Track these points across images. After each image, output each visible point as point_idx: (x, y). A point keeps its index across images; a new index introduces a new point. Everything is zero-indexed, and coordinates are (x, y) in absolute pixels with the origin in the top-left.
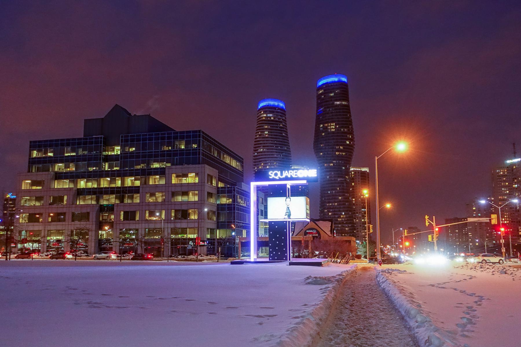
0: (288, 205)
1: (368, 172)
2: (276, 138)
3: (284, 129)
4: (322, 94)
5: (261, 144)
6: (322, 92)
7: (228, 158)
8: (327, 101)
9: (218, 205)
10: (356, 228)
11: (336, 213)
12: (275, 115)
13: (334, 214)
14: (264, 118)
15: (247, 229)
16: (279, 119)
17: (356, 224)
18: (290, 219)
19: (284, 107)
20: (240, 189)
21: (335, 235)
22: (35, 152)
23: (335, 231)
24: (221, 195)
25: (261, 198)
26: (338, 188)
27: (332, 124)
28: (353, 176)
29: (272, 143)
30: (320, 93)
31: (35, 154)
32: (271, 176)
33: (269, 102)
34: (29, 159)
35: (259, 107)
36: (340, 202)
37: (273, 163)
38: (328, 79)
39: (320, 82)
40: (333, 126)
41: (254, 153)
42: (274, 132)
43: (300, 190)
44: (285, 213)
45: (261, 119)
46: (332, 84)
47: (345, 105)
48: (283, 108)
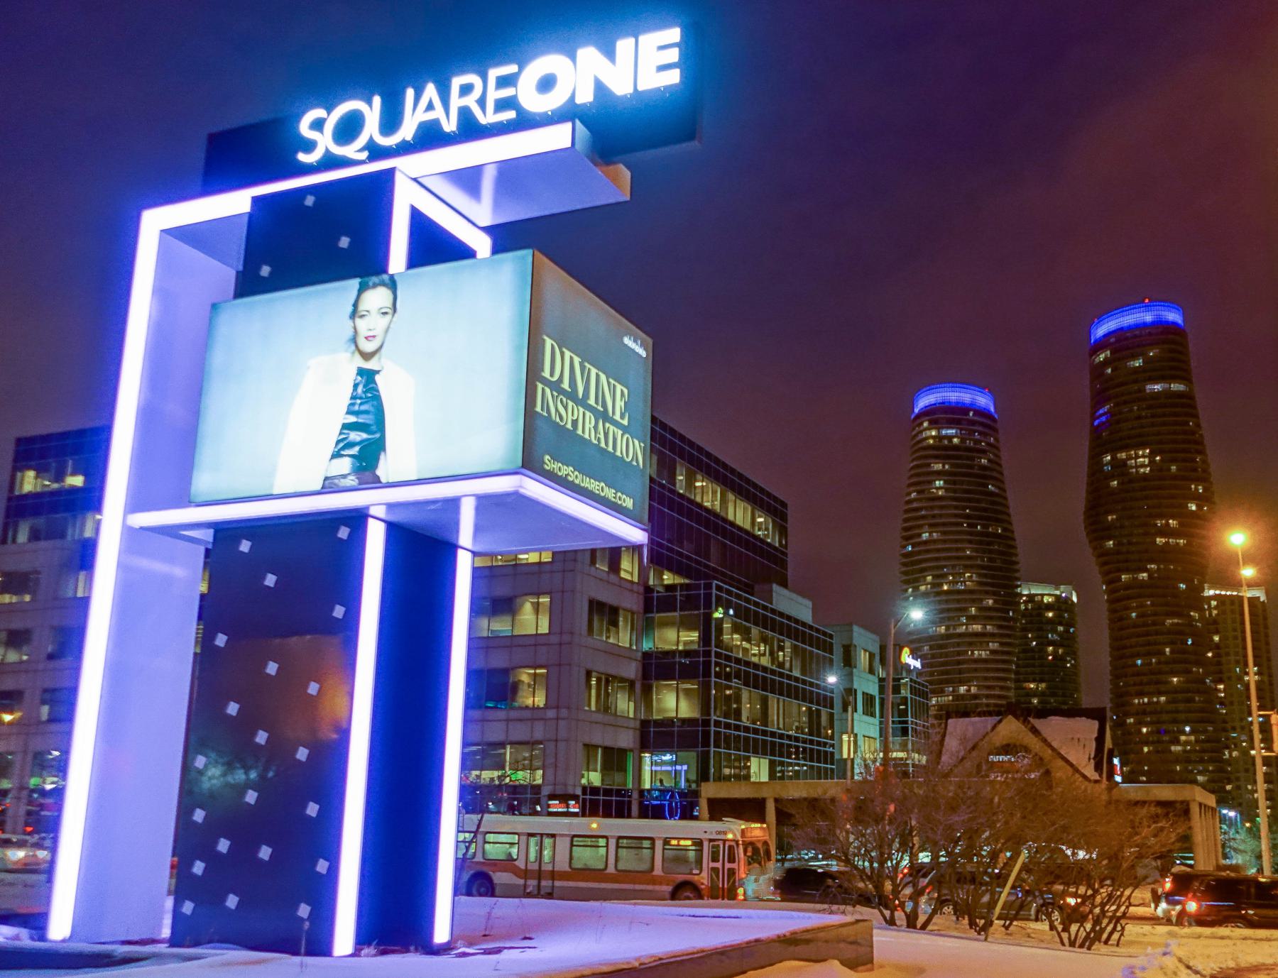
0: (367, 356)
1: (1264, 602)
2: (969, 500)
3: (993, 473)
4: (1106, 363)
5: (923, 517)
6: (1106, 358)
7: (714, 493)
8: (1122, 384)
9: (647, 655)
10: (1233, 777)
11: (1164, 727)
12: (963, 432)
13: (1159, 732)
14: (931, 441)
15: (773, 754)
16: (977, 442)
17: (1230, 765)
18: (376, 483)
19: (992, 409)
20: (765, 608)
21: (1118, 779)
22: (31, 474)
23: (1116, 761)
24: (658, 616)
25: (865, 651)
26: (1168, 650)
27: (1141, 453)
28: (1217, 615)
29: (956, 516)
30: (1101, 362)
31: (30, 482)
32: (309, 146)
33: (945, 394)
34: (10, 499)
35: (916, 410)
36: (1176, 692)
37: (960, 573)
38: (1121, 319)
39: (1099, 330)
40: (1143, 456)
41: (905, 547)
42: (962, 483)
43: (1050, 658)
44: (334, 435)
45: (920, 445)
46: (1137, 332)
47: (1179, 395)
48: (989, 411)
